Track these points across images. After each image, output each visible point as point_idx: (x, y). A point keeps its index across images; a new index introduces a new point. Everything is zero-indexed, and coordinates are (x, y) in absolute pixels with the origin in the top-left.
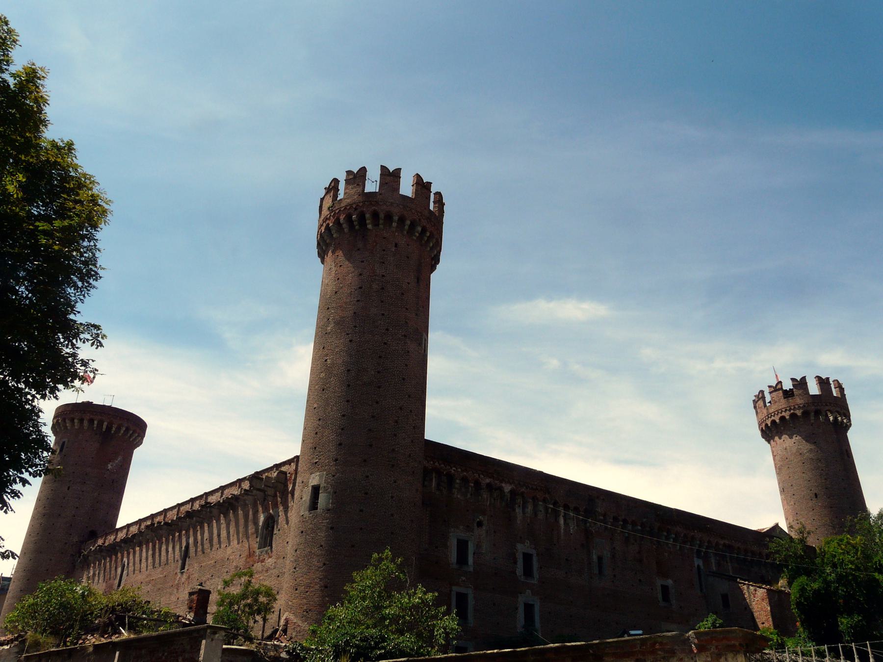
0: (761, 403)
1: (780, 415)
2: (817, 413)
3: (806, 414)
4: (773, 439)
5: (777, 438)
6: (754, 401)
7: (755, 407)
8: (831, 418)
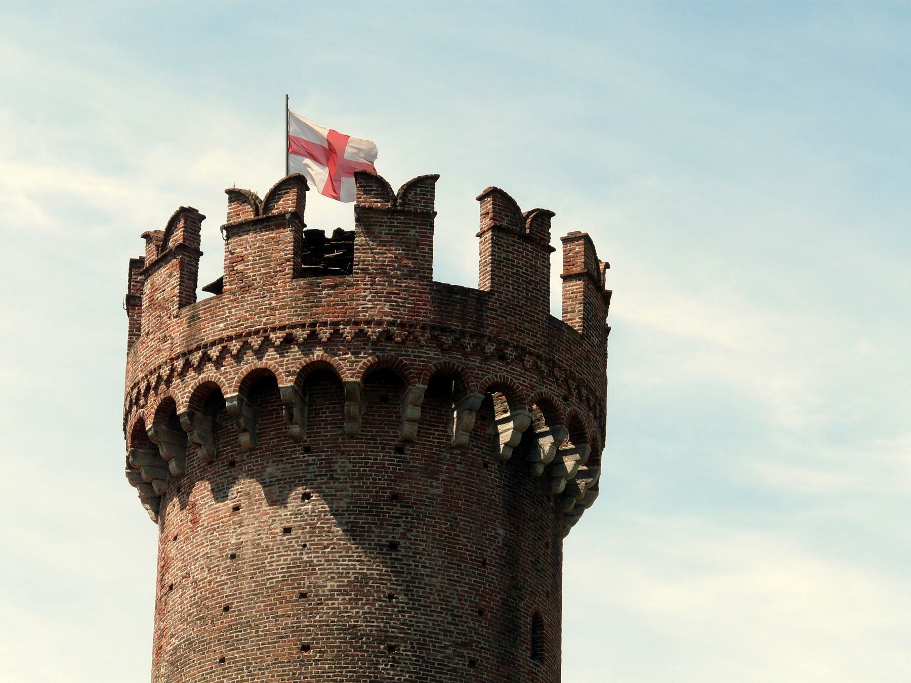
0: (166, 280)
1: (250, 363)
2: (444, 389)
3: (384, 380)
4: (183, 489)
5: (202, 491)
6: (135, 264)
7: (133, 302)
8: (506, 433)
